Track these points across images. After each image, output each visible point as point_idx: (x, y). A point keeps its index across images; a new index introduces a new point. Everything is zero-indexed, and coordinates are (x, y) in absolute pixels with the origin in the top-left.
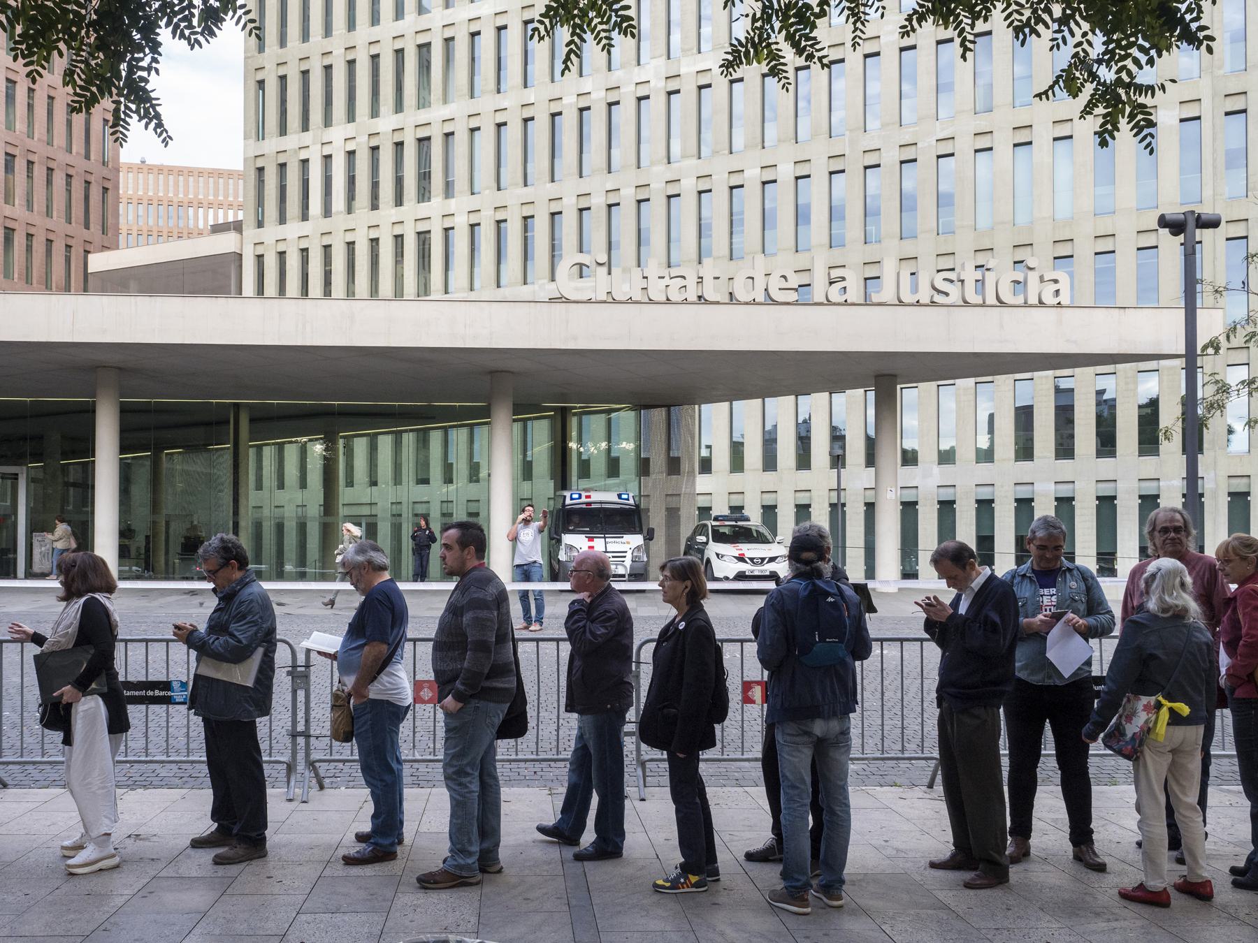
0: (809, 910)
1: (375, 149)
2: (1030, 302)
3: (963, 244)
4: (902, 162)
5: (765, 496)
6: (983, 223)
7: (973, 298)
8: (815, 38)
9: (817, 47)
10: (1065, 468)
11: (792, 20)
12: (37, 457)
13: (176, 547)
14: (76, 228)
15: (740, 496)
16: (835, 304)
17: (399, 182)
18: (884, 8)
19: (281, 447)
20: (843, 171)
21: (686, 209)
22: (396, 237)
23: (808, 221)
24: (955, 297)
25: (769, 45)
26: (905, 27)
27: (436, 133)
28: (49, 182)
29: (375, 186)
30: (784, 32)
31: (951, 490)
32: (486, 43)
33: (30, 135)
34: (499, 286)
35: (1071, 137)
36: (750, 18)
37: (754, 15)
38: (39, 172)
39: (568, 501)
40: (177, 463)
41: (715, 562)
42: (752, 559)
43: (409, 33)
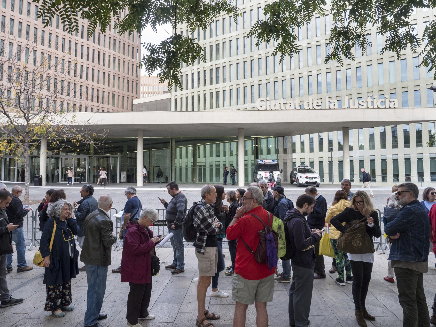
0: (344, 284)
1: (205, 71)
2: (386, 107)
3: (365, 91)
4: (346, 69)
5: (311, 159)
6: (370, 85)
7: (370, 106)
8: (351, 53)
9: (351, 55)
10: (395, 151)
11: (344, 48)
12: (122, 151)
13: (155, 175)
14: (130, 93)
15: (304, 159)
16: (332, 109)
17: (211, 79)
18: (372, 44)
19: (181, 148)
20: (330, 72)
21: (287, 84)
22: (211, 93)
23: (321, 86)
24: (365, 106)
25: (338, 55)
26: (381, 52)
27: (221, 66)
28: (123, 82)
29: (205, 80)
30: (342, 51)
31: (363, 157)
32: (234, 43)
33: (119, 71)
34: (238, 105)
35: (394, 61)
36: (333, 49)
37: (334, 48)
38: (121, 80)
39: (259, 163)
40: (155, 152)
41: (299, 179)
42: (310, 178)
43: (214, 41)
